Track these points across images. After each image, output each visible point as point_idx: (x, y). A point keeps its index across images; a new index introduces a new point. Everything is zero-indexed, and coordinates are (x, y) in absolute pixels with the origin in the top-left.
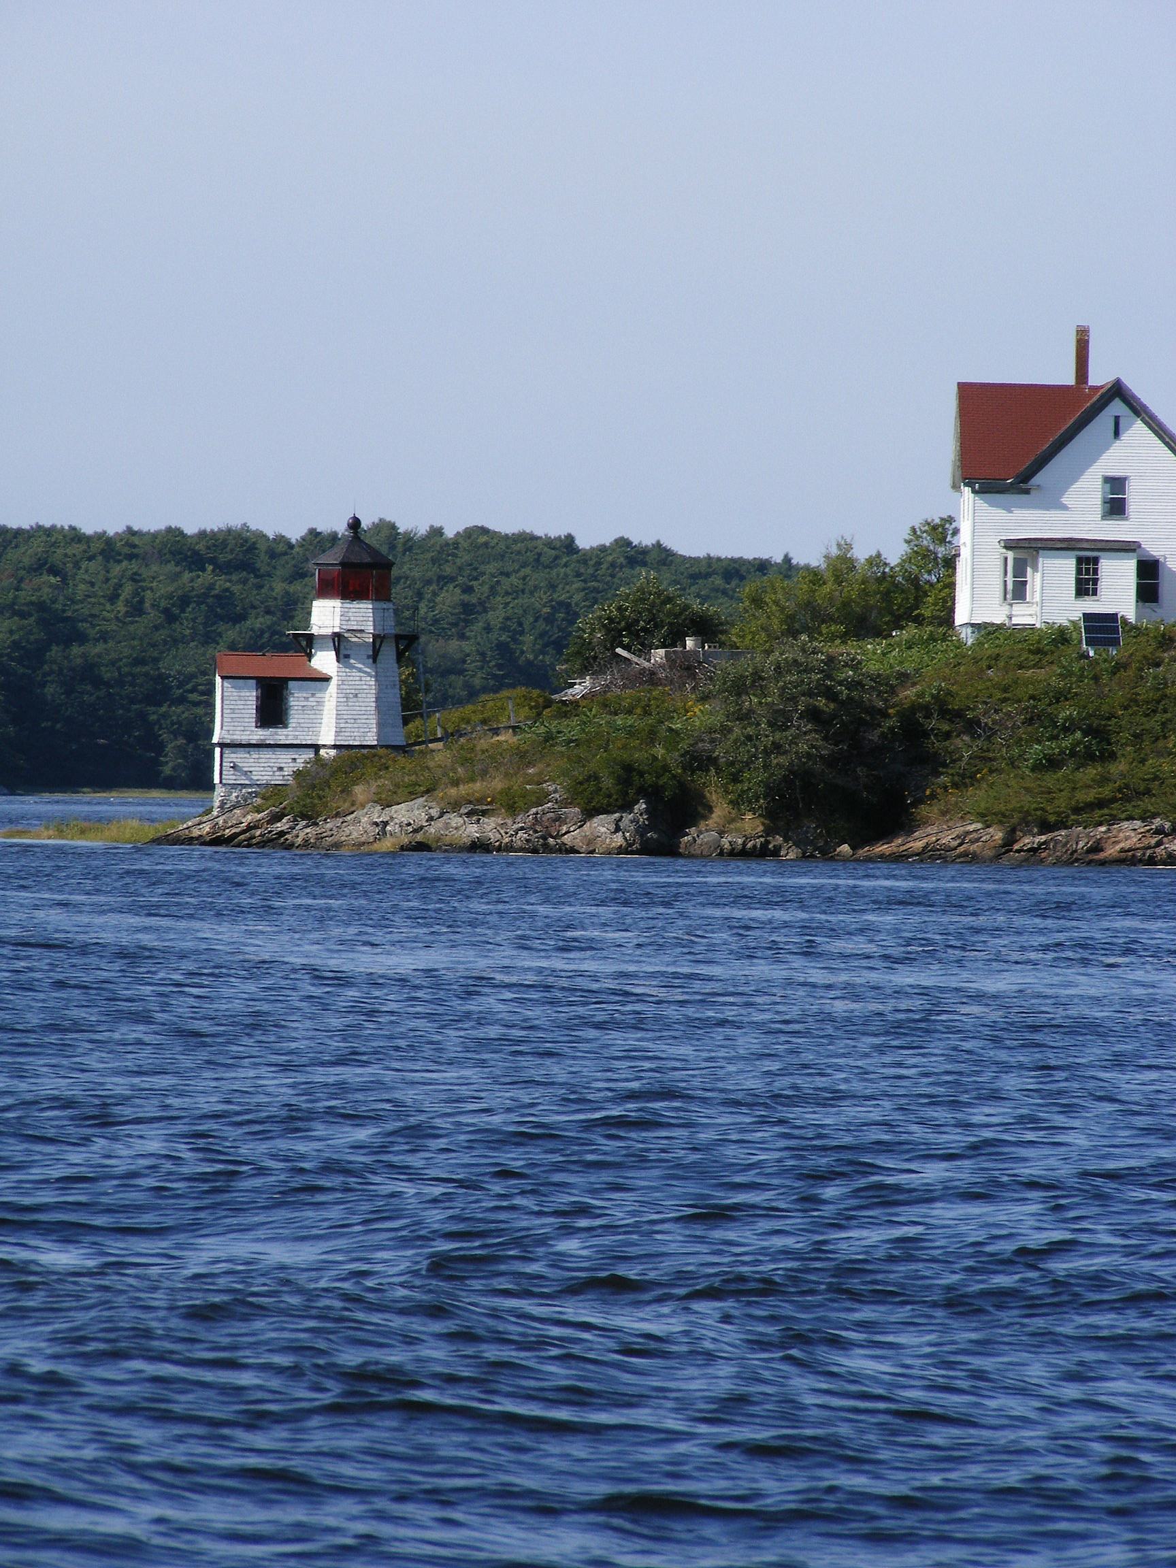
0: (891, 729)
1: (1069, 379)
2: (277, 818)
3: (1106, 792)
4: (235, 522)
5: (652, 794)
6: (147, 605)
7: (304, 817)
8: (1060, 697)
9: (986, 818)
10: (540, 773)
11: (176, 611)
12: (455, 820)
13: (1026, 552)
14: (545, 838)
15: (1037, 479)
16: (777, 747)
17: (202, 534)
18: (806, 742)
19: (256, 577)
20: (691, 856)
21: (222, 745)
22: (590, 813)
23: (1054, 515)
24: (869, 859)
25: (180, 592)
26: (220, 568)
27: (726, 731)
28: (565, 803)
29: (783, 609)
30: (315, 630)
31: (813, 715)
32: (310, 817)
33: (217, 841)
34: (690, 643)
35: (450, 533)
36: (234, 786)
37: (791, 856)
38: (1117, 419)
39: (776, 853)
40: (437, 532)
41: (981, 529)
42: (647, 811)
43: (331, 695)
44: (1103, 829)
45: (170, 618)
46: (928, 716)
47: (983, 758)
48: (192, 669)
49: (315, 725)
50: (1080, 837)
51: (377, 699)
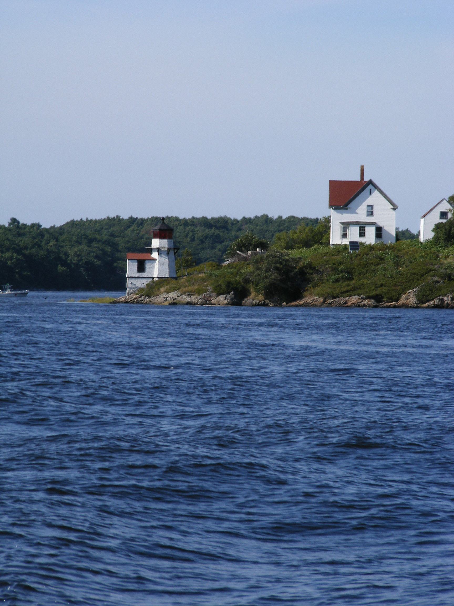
0: (297, 272)
1: (359, 179)
2: (141, 296)
3: (349, 288)
4: (223, 215)
5: (235, 290)
6: (196, 239)
7: (148, 296)
8: (340, 263)
9: (319, 295)
10: (207, 284)
11: (204, 240)
12: (184, 297)
13: (346, 225)
14: (206, 301)
15: (349, 206)
16: (266, 277)
17: (213, 219)
18: (274, 276)
19: (227, 230)
20: (245, 306)
21: (128, 277)
22: (219, 294)
23: (354, 215)
24: (289, 306)
25: (205, 235)
26: (217, 228)
27: (254, 272)
28: (213, 292)
29: (285, 240)
30: (152, 247)
31: (276, 268)
32: (149, 296)
33: (127, 302)
34: (258, 250)
35: (284, 218)
36: (131, 288)
37: (271, 305)
38: (370, 190)
39: (267, 304)
40: (280, 217)
41: (337, 219)
42: (233, 294)
43: (157, 264)
44: (348, 298)
45: (202, 242)
46: (306, 269)
47: (321, 280)
48: (208, 256)
49: (152, 272)
50: (342, 300)
51: (169, 265)
